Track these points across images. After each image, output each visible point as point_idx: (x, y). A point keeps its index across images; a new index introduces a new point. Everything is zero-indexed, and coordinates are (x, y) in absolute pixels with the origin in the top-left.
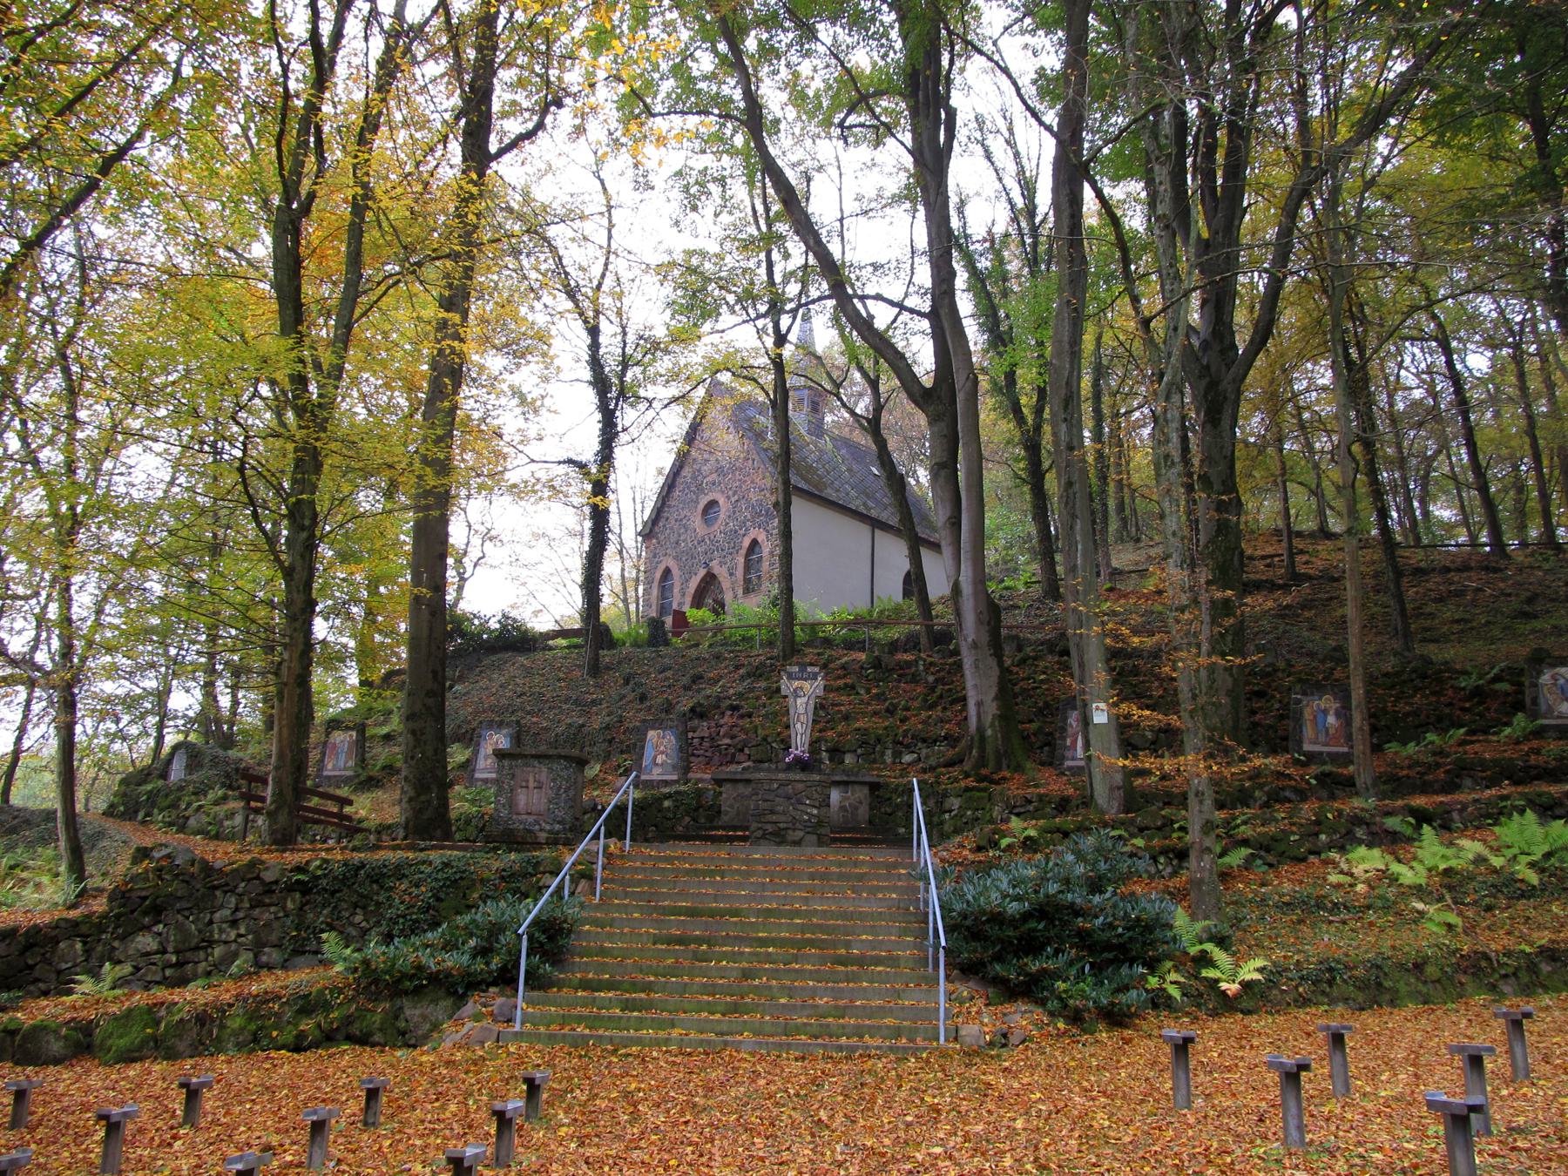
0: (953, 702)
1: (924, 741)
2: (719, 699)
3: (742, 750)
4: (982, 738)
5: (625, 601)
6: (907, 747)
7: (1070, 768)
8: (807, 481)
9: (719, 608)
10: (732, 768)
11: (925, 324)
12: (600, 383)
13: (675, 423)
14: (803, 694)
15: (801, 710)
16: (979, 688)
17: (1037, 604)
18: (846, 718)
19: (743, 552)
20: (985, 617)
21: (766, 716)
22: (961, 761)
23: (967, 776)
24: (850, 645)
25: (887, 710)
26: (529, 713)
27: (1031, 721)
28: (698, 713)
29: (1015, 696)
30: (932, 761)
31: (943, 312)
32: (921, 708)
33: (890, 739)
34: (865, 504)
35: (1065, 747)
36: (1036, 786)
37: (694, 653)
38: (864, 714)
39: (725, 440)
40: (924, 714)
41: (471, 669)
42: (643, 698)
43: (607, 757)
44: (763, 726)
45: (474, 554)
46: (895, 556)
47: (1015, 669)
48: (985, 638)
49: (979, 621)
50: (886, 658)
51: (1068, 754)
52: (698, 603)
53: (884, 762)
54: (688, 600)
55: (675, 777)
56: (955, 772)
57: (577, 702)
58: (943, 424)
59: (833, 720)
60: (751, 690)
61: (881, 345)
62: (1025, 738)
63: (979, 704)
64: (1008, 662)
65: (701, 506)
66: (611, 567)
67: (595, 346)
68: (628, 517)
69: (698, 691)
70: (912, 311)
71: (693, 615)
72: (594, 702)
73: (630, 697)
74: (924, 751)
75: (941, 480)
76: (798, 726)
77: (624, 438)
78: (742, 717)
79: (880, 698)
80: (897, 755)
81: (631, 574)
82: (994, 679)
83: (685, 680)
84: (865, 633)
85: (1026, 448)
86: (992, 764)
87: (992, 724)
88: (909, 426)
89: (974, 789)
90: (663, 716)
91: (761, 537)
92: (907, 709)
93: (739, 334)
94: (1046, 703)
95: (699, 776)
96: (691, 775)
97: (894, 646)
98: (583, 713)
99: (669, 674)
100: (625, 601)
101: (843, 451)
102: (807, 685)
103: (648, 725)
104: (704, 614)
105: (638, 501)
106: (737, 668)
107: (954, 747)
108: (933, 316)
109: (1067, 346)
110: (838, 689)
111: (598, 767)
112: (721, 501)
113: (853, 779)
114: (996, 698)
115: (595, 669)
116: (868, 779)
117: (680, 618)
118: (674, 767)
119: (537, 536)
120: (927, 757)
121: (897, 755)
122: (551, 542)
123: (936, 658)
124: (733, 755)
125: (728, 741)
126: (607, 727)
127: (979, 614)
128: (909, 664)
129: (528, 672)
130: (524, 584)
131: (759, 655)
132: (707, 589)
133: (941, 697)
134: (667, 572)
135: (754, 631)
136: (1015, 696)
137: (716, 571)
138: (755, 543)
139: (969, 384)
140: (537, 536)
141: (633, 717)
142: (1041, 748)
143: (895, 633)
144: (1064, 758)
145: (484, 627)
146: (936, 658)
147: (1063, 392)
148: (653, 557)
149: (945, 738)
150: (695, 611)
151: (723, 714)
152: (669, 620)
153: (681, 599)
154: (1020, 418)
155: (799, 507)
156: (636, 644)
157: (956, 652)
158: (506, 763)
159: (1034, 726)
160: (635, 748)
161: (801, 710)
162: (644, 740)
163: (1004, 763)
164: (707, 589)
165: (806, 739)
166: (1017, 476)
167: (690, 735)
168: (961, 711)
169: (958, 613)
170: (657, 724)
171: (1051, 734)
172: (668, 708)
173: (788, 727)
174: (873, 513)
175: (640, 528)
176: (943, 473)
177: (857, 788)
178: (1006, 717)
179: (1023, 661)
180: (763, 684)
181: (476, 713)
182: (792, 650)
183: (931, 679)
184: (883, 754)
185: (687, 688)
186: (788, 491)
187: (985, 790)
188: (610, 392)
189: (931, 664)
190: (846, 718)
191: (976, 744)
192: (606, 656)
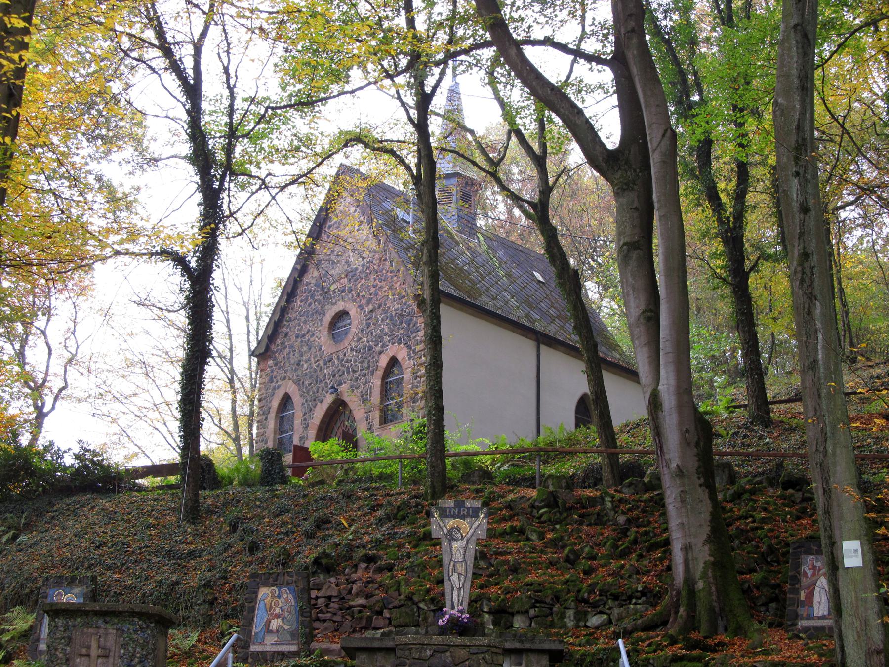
0: (652, 548)
1: (616, 597)
2: (351, 548)
3: (380, 613)
4: (692, 592)
5: (237, 440)
6: (594, 605)
7: (806, 630)
8: (457, 287)
9: (350, 440)
10: (369, 634)
11: (607, 75)
12: (201, 158)
13: (298, 208)
14: (460, 537)
15: (458, 557)
16: (686, 531)
17: (743, 432)
18: (514, 570)
19: (380, 373)
20: (693, 437)
21: (411, 569)
22: (665, 623)
23: (673, 641)
24: (516, 482)
25: (567, 560)
26: (109, 568)
27: (752, 570)
28: (324, 565)
29: (731, 538)
30: (627, 624)
31: (632, 55)
32: (611, 556)
33: (572, 596)
34: (527, 316)
35: (799, 603)
36: (766, 653)
37: (319, 491)
38: (538, 565)
39: (356, 230)
40: (614, 564)
41: (40, 515)
42: (253, 548)
43: (208, 622)
44: (407, 582)
45: (56, 384)
46: (568, 380)
47: (728, 506)
48: (692, 464)
49: (685, 442)
50: (563, 494)
51: (802, 611)
52: (324, 434)
53: (564, 626)
54: (312, 433)
55: (294, 648)
56: (657, 636)
57: (170, 554)
58: (633, 195)
59: (497, 572)
60: (392, 536)
61: (551, 97)
62: (747, 592)
63: (687, 549)
64: (720, 497)
65: (328, 318)
66: (215, 398)
67: (195, 113)
68: (239, 321)
69: (325, 538)
70: (590, 58)
71: (315, 447)
72: (192, 554)
73: (239, 546)
74: (616, 611)
75: (633, 263)
76: (455, 577)
77: (232, 227)
78: (380, 570)
79: (556, 544)
80: (581, 616)
81: (244, 410)
82: (705, 515)
83: (307, 525)
84: (535, 467)
85: (726, 241)
86: (704, 627)
87: (704, 575)
88: (589, 201)
89: (682, 658)
90: (279, 570)
91: (402, 354)
92: (593, 558)
93: (374, 106)
94: (770, 547)
95: (325, 645)
96: (314, 645)
97: (571, 482)
98: (179, 567)
99: (286, 517)
100: (237, 440)
101: (500, 253)
102: (464, 524)
103: (258, 580)
104: (332, 448)
105: (252, 317)
106: (374, 509)
107: (654, 605)
108: (618, 62)
109: (796, 81)
110: (504, 534)
111: (195, 636)
112: (353, 311)
113: (528, 646)
114: (708, 541)
115: (194, 513)
116: (546, 646)
117: (302, 453)
118: (293, 635)
119: (130, 364)
120: (620, 618)
121: (581, 616)
122: (148, 371)
123: (626, 493)
124: (369, 619)
125: (361, 601)
126: (208, 585)
127: (684, 433)
128: (592, 501)
129: (111, 517)
130: (114, 421)
131: (400, 493)
132: (335, 421)
133: (635, 542)
134: (286, 400)
135: (395, 467)
136: (731, 538)
137: (346, 398)
138: (394, 362)
139: (666, 142)
140: (130, 364)
141: (240, 571)
142: (766, 604)
143: (569, 467)
144: (796, 616)
145: (56, 467)
146: (626, 493)
147: (793, 138)
148: (269, 382)
149: (643, 594)
150: (321, 444)
151: (356, 567)
152: (288, 459)
153: (304, 431)
154: (717, 205)
155: (452, 321)
156: (246, 482)
157: (656, 484)
158: (60, 622)
159: (756, 577)
160: (242, 612)
161: (458, 557)
162: (253, 600)
163: (721, 623)
164: (335, 421)
165: (465, 595)
166: (716, 275)
167: (314, 594)
168: (661, 560)
169: (658, 432)
170: (271, 580)
171: (778, 586)
172: (286, 560)
173: (440, 582)
174: (539, 327)
175: (254, 345)
176: (635, 255)
177: (533, 658)
178: (721, 565)
179: (737, 496)
180: (407, 529)
181: (43, 569)
182: (442, 486)
183: (622, 519)
184: (562, 616)
185: (309, 535)
186: (433, 302)
187: (699, 659)
188: (213, 168)
189: (621, 501)
190: (514, 570)
191: (684, 601)
192: (208, 497)
